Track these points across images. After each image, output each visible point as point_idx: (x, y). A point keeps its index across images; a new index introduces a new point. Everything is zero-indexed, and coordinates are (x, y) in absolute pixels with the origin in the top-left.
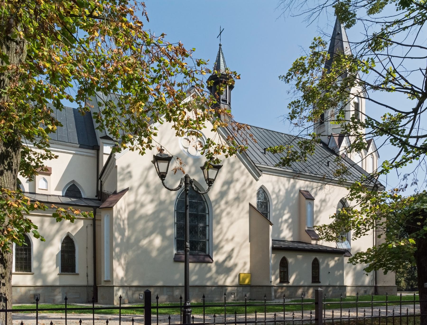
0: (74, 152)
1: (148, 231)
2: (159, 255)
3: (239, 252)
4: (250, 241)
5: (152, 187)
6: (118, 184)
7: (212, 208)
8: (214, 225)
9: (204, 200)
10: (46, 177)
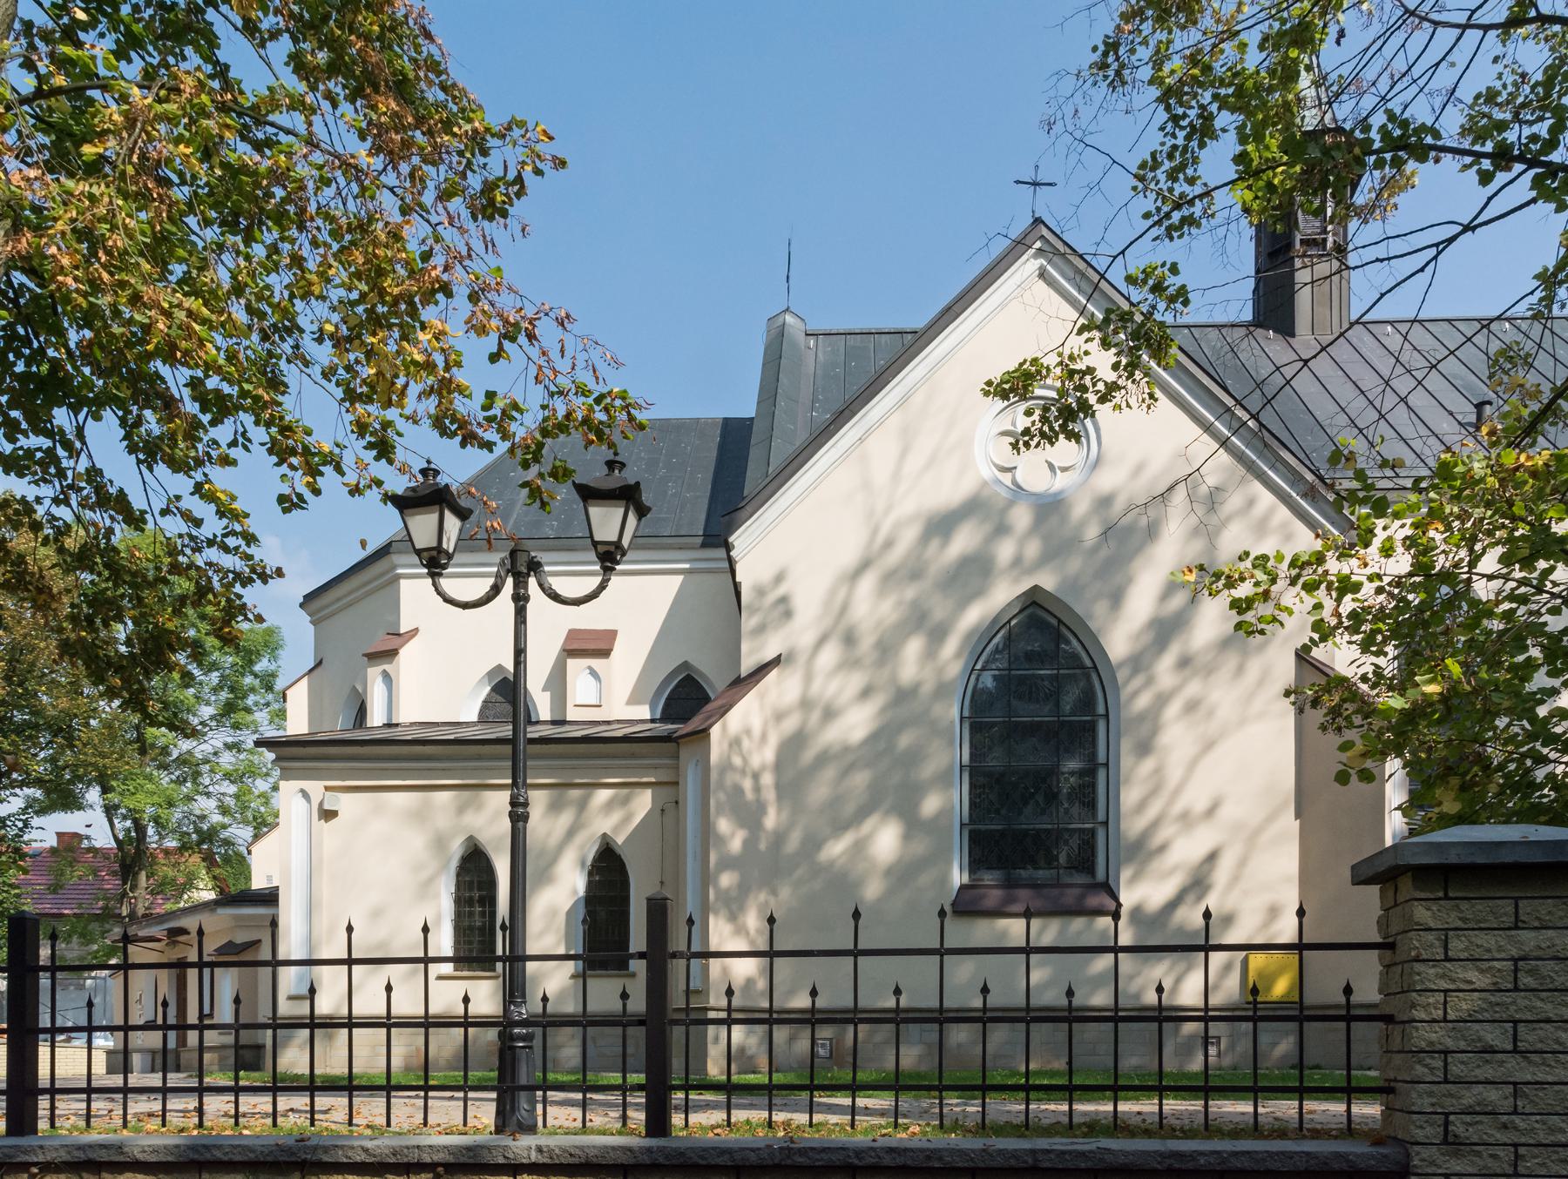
0: (687, 566)
1: (850, 808)
2: (889, 894)
3: (1242, 863)
4: (1298, 816)
5: (867, 643)
6: (745, 647)
7: (1117, 689)
8: (1126, 761)
9: (1088, 663)
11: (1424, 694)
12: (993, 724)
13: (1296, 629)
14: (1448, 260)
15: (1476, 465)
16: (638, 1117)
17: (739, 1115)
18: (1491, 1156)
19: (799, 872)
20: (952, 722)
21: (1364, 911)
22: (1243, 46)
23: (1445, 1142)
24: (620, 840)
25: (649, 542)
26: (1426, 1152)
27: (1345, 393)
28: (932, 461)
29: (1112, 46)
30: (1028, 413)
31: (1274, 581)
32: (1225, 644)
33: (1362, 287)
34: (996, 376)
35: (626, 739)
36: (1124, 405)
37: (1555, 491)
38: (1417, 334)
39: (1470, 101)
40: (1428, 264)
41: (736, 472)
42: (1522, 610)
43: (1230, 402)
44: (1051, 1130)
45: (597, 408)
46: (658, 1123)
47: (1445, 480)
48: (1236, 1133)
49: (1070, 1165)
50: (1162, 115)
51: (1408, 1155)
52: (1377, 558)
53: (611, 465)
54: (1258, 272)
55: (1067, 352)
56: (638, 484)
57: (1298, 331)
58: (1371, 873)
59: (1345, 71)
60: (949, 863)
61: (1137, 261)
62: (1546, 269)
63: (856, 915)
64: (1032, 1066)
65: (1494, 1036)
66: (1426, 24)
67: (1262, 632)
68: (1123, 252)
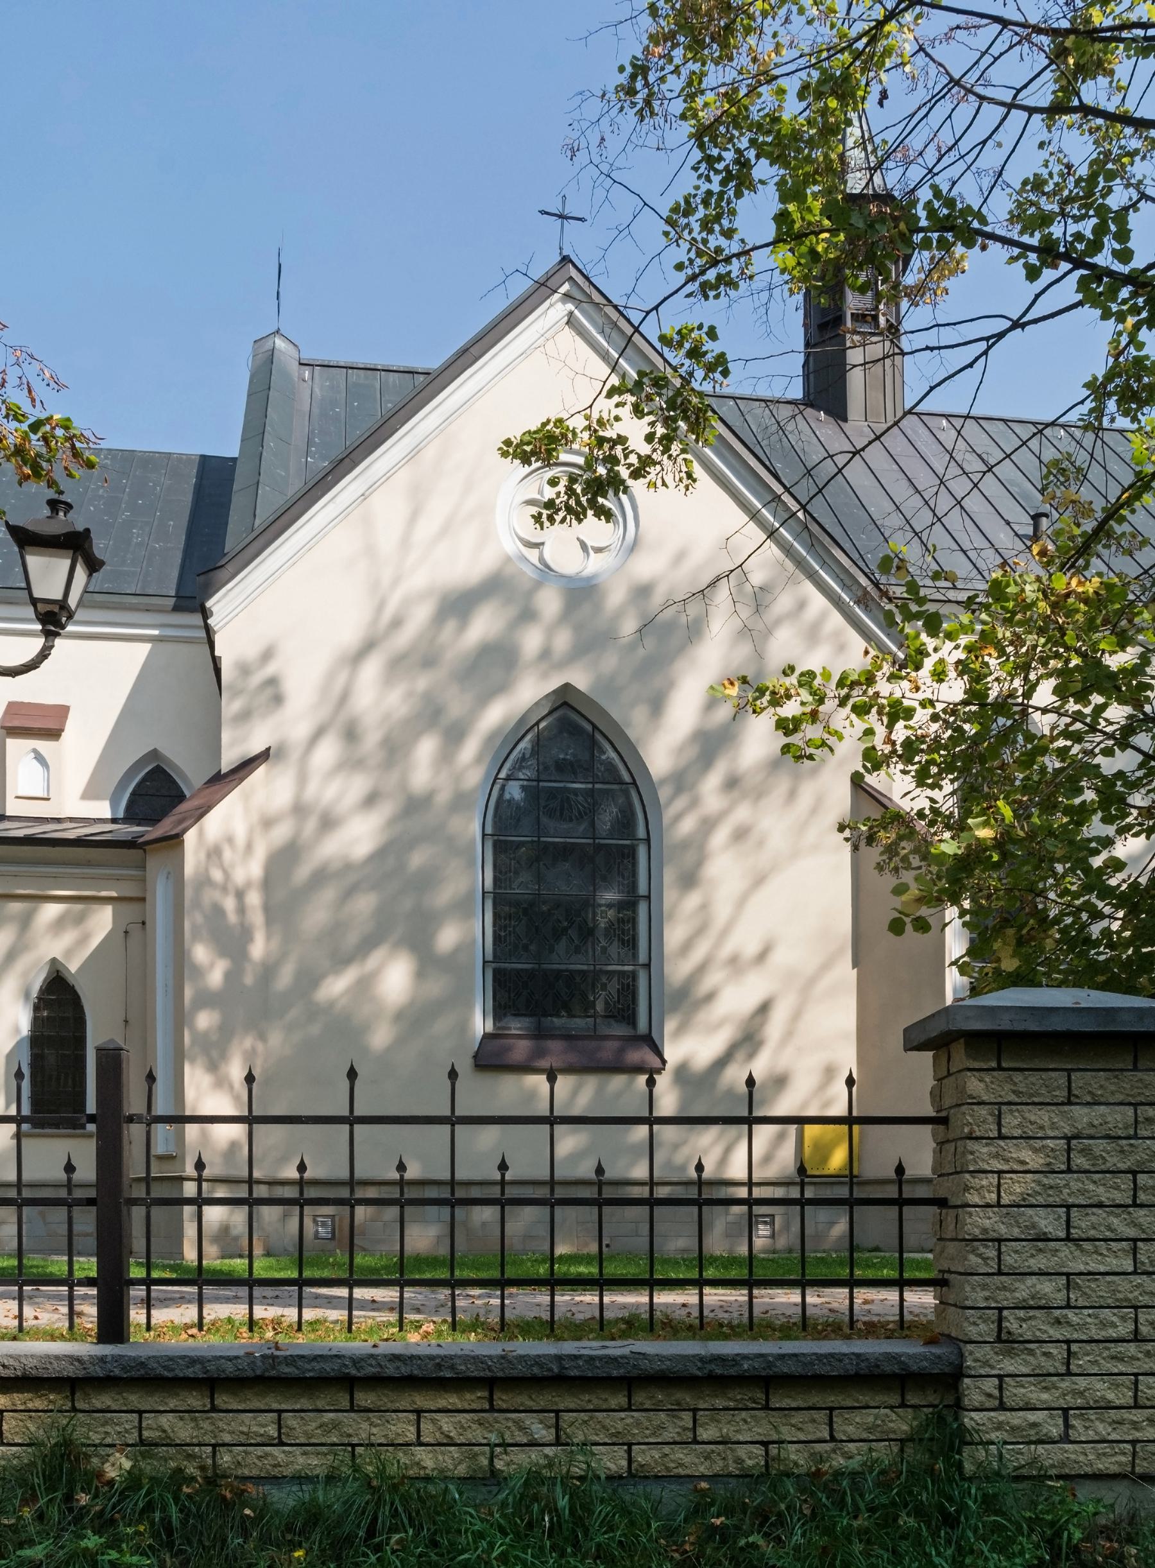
0: (156, 632)
1: (352, 938)
2: (400, 1041)
3: (796, 1016)
4: (855, 964)
5: (372, 739)
6: (226, 736)
8: (670, 895)
9: (627, 778)
10: (42, 745)
11: (978, 839)
12: (520, 845)
13: (847, 755)
14: (1003, 358)
15: (1028, 588)
16: (90, 1311)
17: (215, 1312)
18: (1045, 1354)
19: (293, 1013)
20: (474, 840)
21: (915, 1081)
22: (781, 92)
23: (999, 1340)
24: (73, 966)
25: (107, 600)
26: (982, 1352)
27: (900, 491)
28: (446, 530)
29: (640, 69)
30: (553, 482)
31: (821, 701)
32: (774, 766)
33: (916, 373)
34: (516, 435)
35: (79, 842)
36: (659, 483)
37: (1105, 622)
38: (971, 427)
39: (1018, 187)
40: (977, 359)
41: (216, 524)
42: (1076, 749)
43: (778, 489)
44: (577, 1330)
45: (33, 437)
46: (113, 1326)
47: (997, 600)
48: (786, 1331)
49: (600, 1373)
50: (697, 155)
51: (961, 1355)
52: (929, 681)
53: (54, 504)
54: (807, 345)
55: (595, 416)
56: (87, 531)
57: (850, 416)
58: (923, 1038)
59: (891, 136)
60: (470, 1007)
61: (672, 320)
62: (1095, 379)
63: (352, 1074)
64: (561, 1250)
65: (1048, 1222)
66: (972, 98)
67: (811, 757)
68: (656, 308)
